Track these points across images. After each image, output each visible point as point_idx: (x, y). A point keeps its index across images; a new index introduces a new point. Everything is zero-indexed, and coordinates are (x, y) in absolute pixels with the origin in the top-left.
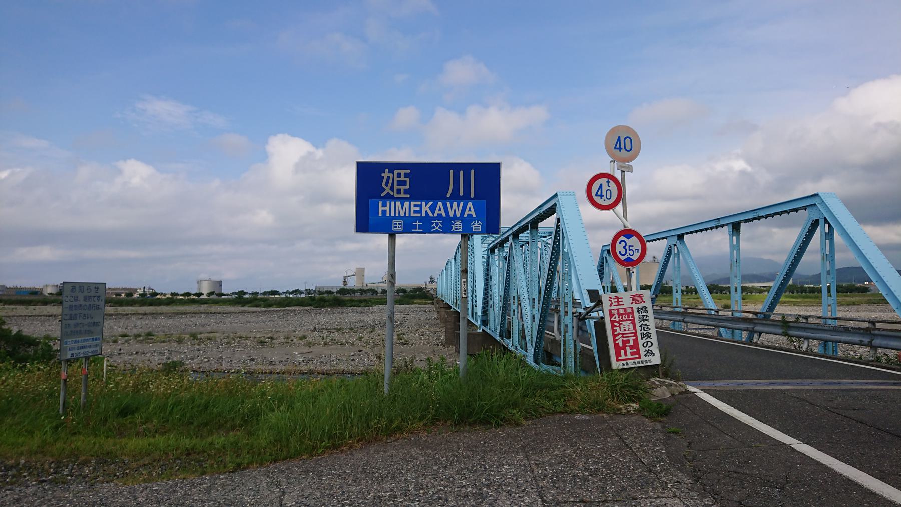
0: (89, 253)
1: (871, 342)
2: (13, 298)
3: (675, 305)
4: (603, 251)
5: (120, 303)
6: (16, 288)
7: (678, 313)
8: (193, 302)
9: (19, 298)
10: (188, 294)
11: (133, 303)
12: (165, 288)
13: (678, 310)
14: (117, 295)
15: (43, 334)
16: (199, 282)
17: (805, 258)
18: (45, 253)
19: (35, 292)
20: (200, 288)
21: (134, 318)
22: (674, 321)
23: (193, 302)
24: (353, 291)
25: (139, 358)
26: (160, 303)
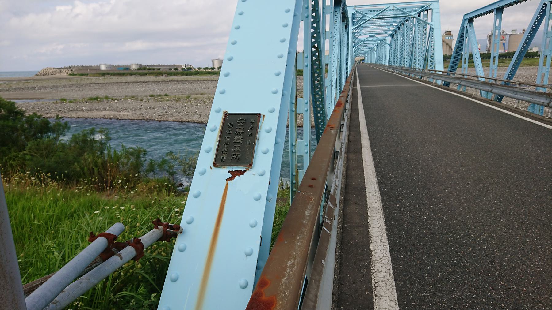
0: (162, 45)
1: (548, 104)
2: (116, 72)
3: (538, 82)
4: (464, 20)
5: (170, 74)
6: (119, 66)
7: (541, 94)
8: (209, 73)
9: (118, 72)
10: (207, 68)
11: (177, 74)
12: (196, 66)
13: (541, 90)
14: (170, 69)
15: (105, 95)
16: (213, 61)
17: (535, 40)
18: (139, 45)
19: (127, 68)
20: (213, 64)
21: (172, 83)
22: (534, 103)
23: (209, 73)
24: (374, 64)
25: (151, 112)
26: (197, 73)
